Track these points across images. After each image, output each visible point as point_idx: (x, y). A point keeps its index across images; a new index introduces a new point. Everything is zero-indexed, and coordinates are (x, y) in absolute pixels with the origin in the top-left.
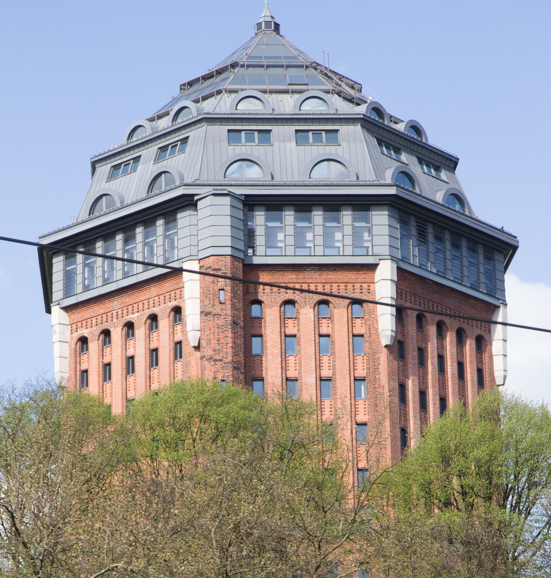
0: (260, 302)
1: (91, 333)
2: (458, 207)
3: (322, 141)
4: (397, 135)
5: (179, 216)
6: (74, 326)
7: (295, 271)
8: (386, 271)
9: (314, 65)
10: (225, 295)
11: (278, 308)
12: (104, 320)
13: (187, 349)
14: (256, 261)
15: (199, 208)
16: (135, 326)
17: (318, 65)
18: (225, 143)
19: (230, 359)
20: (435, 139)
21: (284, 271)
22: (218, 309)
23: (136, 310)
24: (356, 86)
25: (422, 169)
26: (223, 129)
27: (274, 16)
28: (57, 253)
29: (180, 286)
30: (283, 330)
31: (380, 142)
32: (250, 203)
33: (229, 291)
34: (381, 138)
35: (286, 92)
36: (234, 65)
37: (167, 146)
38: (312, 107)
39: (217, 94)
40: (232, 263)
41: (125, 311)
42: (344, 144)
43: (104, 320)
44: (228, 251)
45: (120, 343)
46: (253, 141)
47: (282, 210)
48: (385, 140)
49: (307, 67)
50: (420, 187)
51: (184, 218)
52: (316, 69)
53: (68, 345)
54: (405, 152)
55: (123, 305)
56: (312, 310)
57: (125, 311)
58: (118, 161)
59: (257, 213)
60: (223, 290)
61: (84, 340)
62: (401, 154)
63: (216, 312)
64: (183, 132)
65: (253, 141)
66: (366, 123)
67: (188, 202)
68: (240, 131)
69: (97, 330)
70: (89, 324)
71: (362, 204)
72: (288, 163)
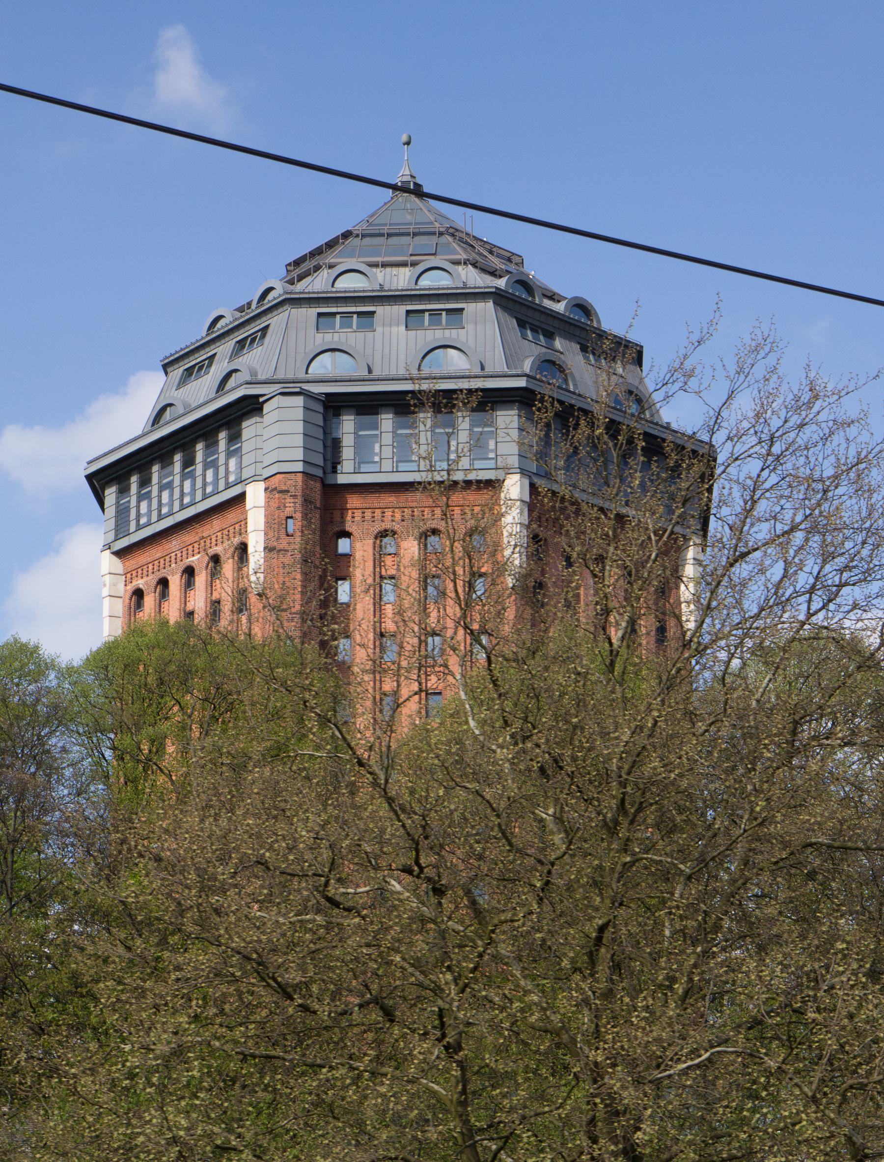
0: (348, 535)
1: (146, 583)
2: (634, 408)
3: (441, 324)
4: (554, 317)
5: (245, 424)
6: (129, 575)
7: (394, 492)
8: (514, 487)
9: (451, 231)
10: (294, 524)
11: (371, 541)
12: (162, 566)
13: (253, 599)
14: (342, 479)
15: (265, 411)
16: (196, 571)
17: (457, 230)
18: (312, 331)
19: (298, 608)
20: (611, 321)
21: (380, 492)
22: (284, 543)
23: (196, 551)
24: (515, 259)
25: (588, 359)
26: (311, 313)
28: (108, 483)
29: (242, 517)
30: (378, 569)
31: (522, 324)
32: (334, 405)
33: (300, 519)
34: (524, 318)
35: (404, 264)
36: (347, 235)
37: (246, 338)
38: (432, 281)
39: (315, 272)
40: (305, 482)
41: (184, 553)
42: (470, 327)
43: (162, 566)
44: (299, 467)
45: (178, 594)
46: (351, 326)
47: (377, 414)
48: (530, 321)
49: (441, 234)
50: (574, 380)
51: (249, 427)
52: (453, 235)
53: (121, 600)
54: (561, 336)
55: (182, 545)
56: (416, 542)
57: (184, 553)
58: (186, 363)
59: (345, 418)
60: (291, 517)
61: (139, 594)
62: (554, 340)
63: (281, 546)
64: (264, 319)
65: (351, 326)
66: (500, 298)
67: (251, 406)
68: (334, 314)
69: (153, 579)
70: (145, 573)
71: (489, 400)
72: (391, 350)
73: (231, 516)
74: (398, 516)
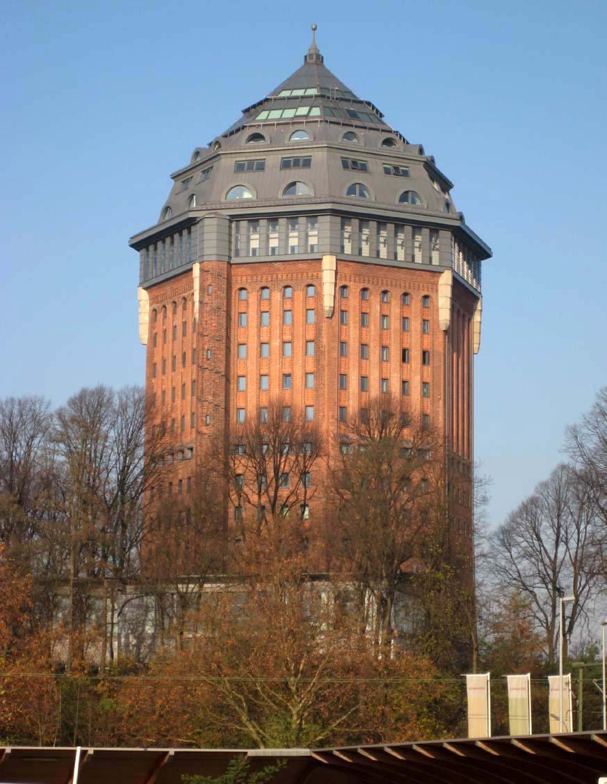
8: (329, 262)
73: (184, 281)
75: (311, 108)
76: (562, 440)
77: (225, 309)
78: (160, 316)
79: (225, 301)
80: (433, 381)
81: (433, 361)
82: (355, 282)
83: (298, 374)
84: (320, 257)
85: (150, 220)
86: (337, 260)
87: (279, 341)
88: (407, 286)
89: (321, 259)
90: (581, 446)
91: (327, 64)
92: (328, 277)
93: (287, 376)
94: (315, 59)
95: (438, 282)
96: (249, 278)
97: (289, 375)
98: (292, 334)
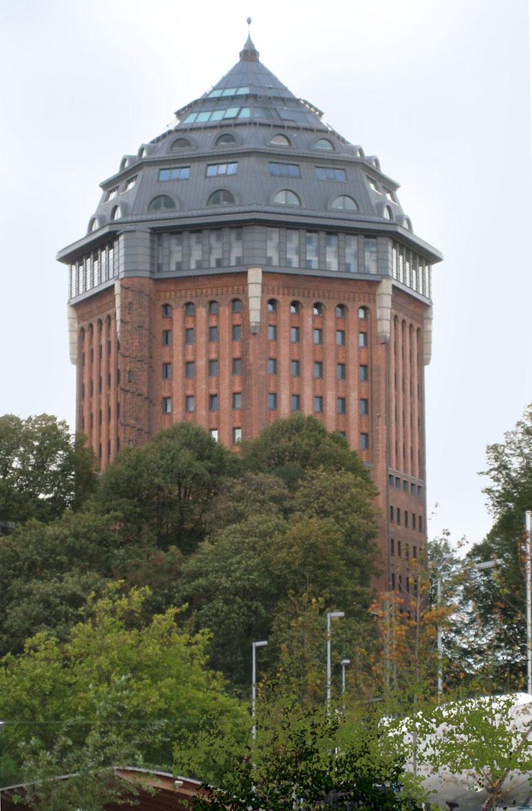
27: (246, 21)
73: (108, 299)
74: (194, 294)
75: (241, 108)
76: (485, 462)
77: (147, 327)
78: (87, 335)
79: (147, 319)
80: (372, 398)
81: (371, 375)
82: (283, 295)
83: (225, 394)
84: (244, 270)
85: (77, 233)
86: (263, 272)
87: (204, 359)
88: (342, 297)
89: (247, 272)
90: (504, 467)
91: (263, 59)
92: (255, 291)
93: (212, 397)
94: (249, 54)
95: (375, 292)
96: (173, 294)
97: (216, 396)
98: (218, 352)
